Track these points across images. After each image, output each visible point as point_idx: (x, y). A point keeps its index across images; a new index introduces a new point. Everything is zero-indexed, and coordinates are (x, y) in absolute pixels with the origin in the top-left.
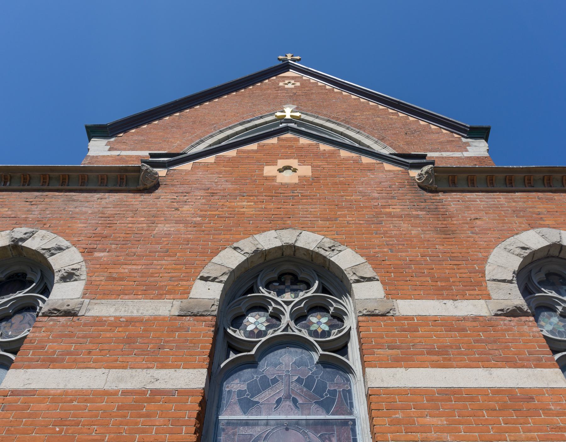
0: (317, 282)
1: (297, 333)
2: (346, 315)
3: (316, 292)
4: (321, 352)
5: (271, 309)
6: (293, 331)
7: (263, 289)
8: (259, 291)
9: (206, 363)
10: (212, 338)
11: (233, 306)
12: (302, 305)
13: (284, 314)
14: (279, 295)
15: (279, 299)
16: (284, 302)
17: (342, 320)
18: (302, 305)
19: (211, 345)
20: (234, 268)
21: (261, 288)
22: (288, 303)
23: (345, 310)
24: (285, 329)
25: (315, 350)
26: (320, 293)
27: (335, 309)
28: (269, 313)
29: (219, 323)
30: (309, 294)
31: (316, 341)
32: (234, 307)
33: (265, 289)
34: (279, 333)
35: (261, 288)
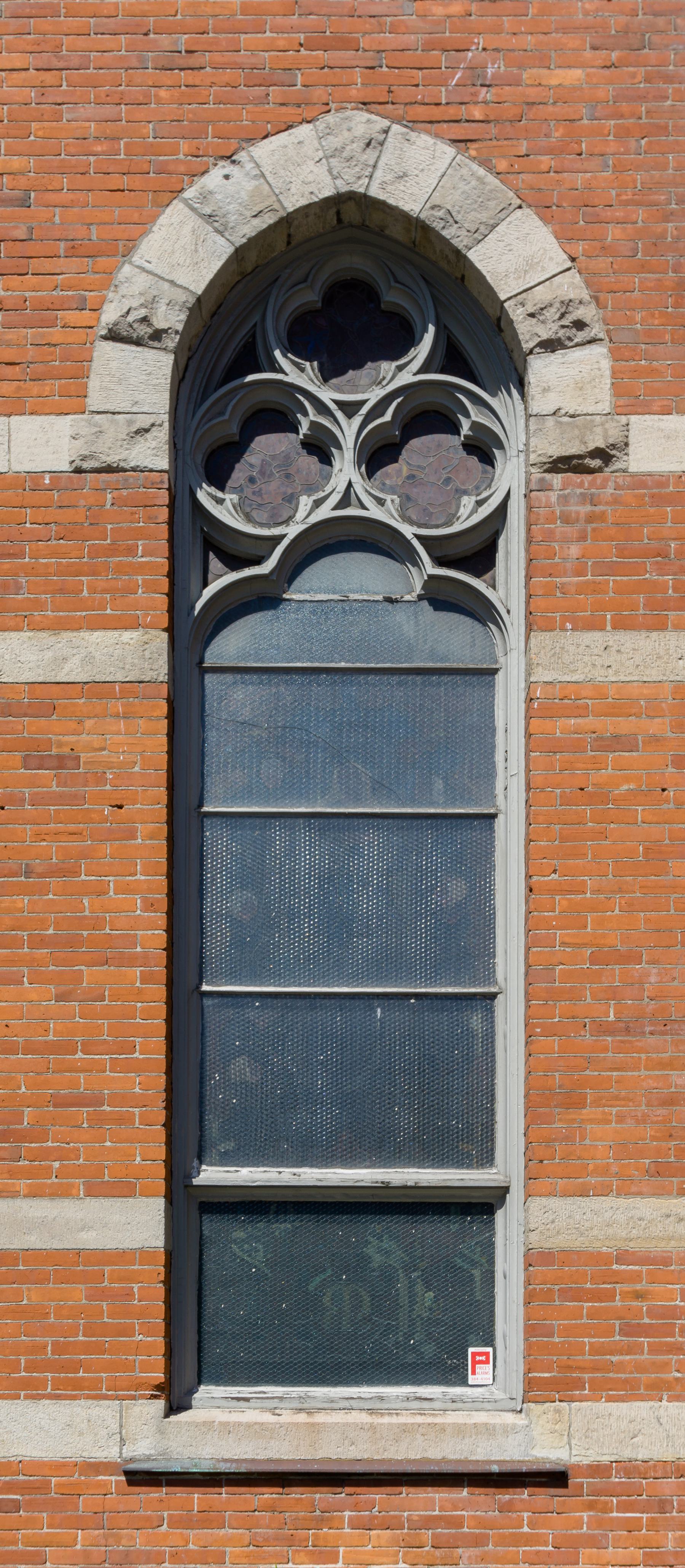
0: (431, 329)
1: (375, 512)
2: (501, 446)
3: (425, 368)
4: (431, 569)
5: (304, 429)
6: (364, 507)
7: (285, 356)
8: (275, 367)
9: (161, 1184)
10: (167, 558)
11: (205, 420)
12: (388, 417)
13: (339, 447)
14: (327, 375)
15: (327, 395)
16: (340, 404)
17: (488, 459)
18: (388, 417)
19: (165, 952)
20: (200, 292)
21: (277, 353)
22: (350, 409)
23: (497, 429)
24: (344, 502)
25: (412, 558)
26: (436, 372)
27: (475, 426)
28: (301, 437)
29: (172, 698)
30: (406, 378)
31: (418, 537)
32: (210, 420)
33: (289, 355)
34: (325, 512)
35: (277, 353)
